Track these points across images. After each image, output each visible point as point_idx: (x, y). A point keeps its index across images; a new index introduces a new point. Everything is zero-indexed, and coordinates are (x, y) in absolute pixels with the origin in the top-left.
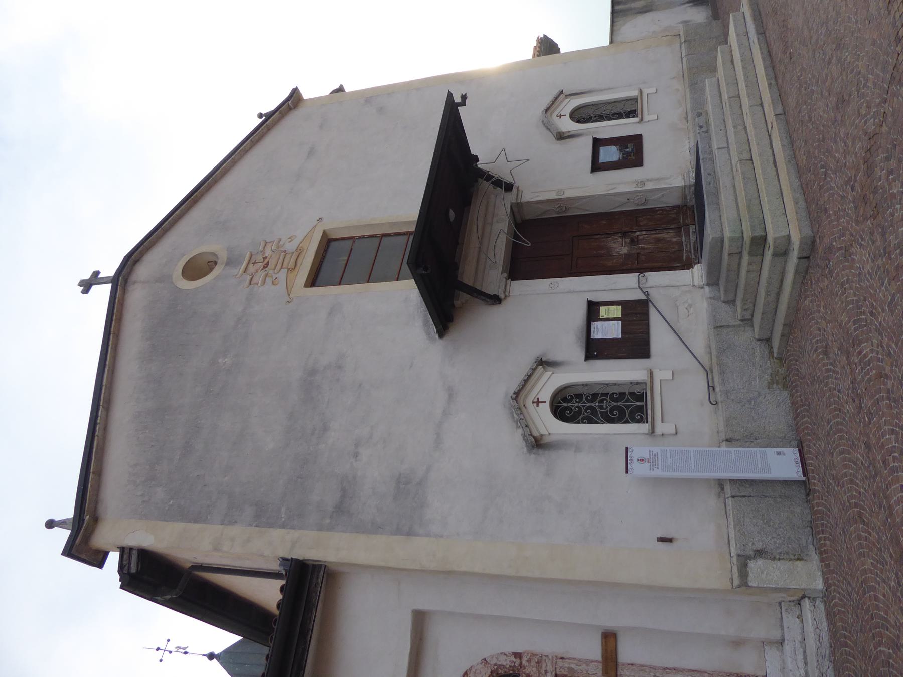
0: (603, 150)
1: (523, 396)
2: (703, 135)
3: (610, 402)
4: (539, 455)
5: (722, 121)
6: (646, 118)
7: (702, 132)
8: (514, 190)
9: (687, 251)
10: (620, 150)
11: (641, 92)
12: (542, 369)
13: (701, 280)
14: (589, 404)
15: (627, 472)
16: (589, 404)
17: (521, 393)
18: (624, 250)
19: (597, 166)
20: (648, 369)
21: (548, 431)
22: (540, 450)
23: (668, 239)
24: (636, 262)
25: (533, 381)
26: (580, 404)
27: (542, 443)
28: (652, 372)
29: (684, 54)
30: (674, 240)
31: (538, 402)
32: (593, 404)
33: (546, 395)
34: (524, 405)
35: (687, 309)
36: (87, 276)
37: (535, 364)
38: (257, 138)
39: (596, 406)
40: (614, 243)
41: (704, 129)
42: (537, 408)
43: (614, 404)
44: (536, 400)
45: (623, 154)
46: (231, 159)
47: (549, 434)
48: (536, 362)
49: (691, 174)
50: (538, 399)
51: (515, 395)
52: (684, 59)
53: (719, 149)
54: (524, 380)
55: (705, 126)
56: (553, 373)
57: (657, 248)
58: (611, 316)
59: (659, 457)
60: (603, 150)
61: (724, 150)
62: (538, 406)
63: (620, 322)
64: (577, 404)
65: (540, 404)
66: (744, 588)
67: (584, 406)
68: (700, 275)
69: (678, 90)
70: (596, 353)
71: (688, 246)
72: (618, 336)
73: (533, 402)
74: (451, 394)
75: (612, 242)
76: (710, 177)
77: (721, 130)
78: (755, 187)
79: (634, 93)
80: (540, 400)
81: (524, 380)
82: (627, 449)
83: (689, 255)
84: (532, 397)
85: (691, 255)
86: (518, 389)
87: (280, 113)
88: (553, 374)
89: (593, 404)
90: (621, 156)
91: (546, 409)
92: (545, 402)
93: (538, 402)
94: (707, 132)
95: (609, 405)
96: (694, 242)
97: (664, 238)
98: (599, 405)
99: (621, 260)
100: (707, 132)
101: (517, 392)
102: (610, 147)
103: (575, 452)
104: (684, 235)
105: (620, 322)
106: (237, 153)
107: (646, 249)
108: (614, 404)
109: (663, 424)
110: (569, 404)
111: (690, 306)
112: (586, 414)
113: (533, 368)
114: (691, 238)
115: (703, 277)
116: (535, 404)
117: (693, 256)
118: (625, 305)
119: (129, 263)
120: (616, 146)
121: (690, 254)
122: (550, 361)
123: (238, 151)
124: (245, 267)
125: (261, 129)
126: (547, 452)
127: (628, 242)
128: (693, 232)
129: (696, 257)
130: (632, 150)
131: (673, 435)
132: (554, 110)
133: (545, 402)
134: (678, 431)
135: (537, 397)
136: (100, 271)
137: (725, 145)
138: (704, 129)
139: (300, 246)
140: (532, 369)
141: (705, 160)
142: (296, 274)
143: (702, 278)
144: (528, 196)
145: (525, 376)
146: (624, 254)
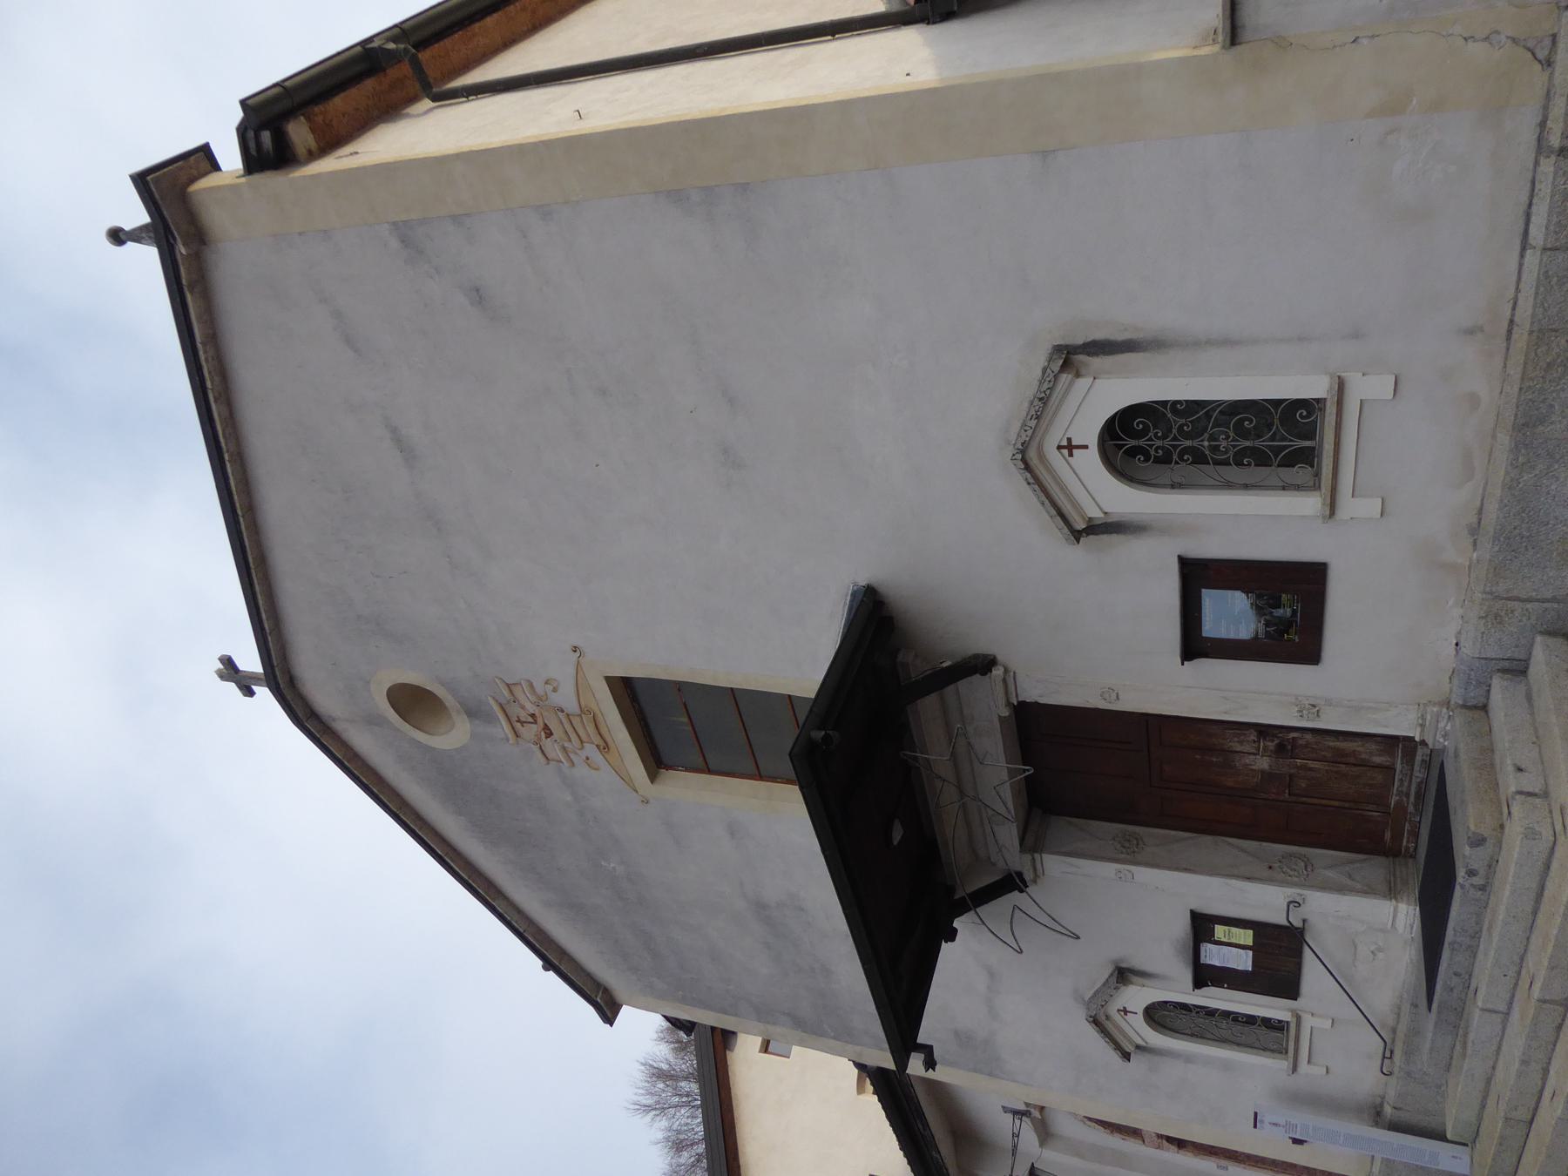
0: (1211, 600)
2: (1472, 891)
5: (1516, 959)
6: (1349, 506)
7: (1472, 885)
8: (997, 672)
9: (1400, 793)
10: (1259, 610)
11: (1341, 387)
13: (1408, 929)
15: (1255, 1126)
18: (1263, 763)
19: (1194, 645)
21: (1101, 509)
23: (1363, 756)
24: (1287, 791)
25: (1051, 413)
28: (1300, 1017)
29: (1537, 234)
30: (1377, 760)
31: (1070, 447)
33: (1088, 430)
34: (1107, 1016)
35: (1372, 952)
36: (232, 687)
38: (217, 379)
40: (1241, 743)
41: (1477, 881)
44: (1065, 443)
45: (1267, 624)
46: (227, 463)
47: (1106, 513)
49: (1441, 725)
50: (1069, 440)
52: (1532, 259)
53: (1483, 1010)
55: (1482, 872)
56: (1095, 378)
57: (1336, 772)
58: (1233, 941)
59: (1298, 1128)
60: (1211, 600)
61: (1494, 1015)
62: (1071, 455)
63: (1250, 953)
64: (1159, 443)
65: (1075, 451)
66: (1486, 44)
68: (1408, 922)
69: (1473, 400)
71: (1406, 784)
72: (1249, 936)
74: (992, 974)
75: (1236, 739)
76: (1455, 980)
77: (1505, 975)
78: (1515, 1159)
79: (1312, 387)
82: (1256, 1114)
83: (1402, 800)
84: (1055, 437)
85: (1408, 803)
87: (192, 288)
90: (1261, 626)
91: (1090, 462)
92: (1086, 447)
93: (1070, 447)
94: (1483, 888)
95: (1234, 446)
96: (1421, 782)
97: (1354, 751)
99: (1255, 780)
100: (1483, 888)
102: (1230, 592)
104: (1402, 759)
105: (1250, 953)
106: (223, 445)
107: (1311, 769)
111: (1380, 950)
114: (1416, 774)
115: (1415, 926)
116: (1065, 452)
117: (1411, 808)
118: (1257, 927)
119: (289, 697)
120: (1247, 593)
121: (1405, 799)
123: (222, 440)
124: (510, 728)
125: (204, 363)
127: (1272, 748)
128: (1423, 760)
129: (1416, 810)
130: (1294, 612)
132: (1043, 435)
133: (1086, 447)
136: (255, 697)
137: (1502, 1007)
138: (1477, 881)
139: (583, 707)
141: (1456, 946)
142: (617, 755)
143: (1412, 928)
144: (1035, 690)
146: (1263, 772)
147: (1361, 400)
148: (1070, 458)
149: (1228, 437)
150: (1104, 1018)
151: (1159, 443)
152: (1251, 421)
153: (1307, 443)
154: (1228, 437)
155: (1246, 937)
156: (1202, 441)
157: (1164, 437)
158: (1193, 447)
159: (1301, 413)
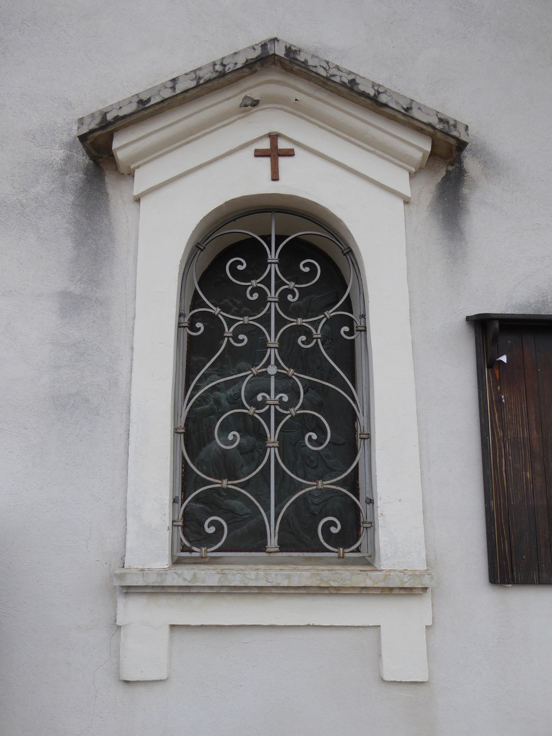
1: (293, 94)
3: (279, 417)
4: (63, 172)
12: (418, 156)
14: (272, 340)
16: (272, 340)
17: (302, 85)
20: (426, 581)
22: (81, 175)
26: (273, 308)
27: (107, 179)
32: (273, 353)
34: (255, 103)
37: (434, 121)
39: (268, 363)
42: (250, 152)
43: (273, 437)
44: (282, 145)
47: (138, 200)
48: (441, 120)
50: (289, 153)
51: (280, 51)
54: (353, 81)
56: (406, 202)
62: (259, 154)
63: (182, 435)
64: (273, 295)
65: (266, 162)
67: (265, 321)
70: (504, 359)
73: (274, 137)
80: (283, 161)
81: (353, 81)
86: (311, 62)
88: (400, 203)
89: (273, 353)
92: (275, 177)
95: (266, 416)
98: (265, 375)
101: (294, 61)
103: (65, 294)
108: (273, 437)
109: (167, 629)
110: (273, 269)
112: (228, 332)
113: (415, 113)
116: (266, 145)
122: (465, 191)
126: (70, 198)
131: (118, 672)
133: (275, 177)
134: (141, 690)
135: (297, 150)
140: (408, 109)
145: (374, 85)
147: (379, 626)
148: (252, 153)
149: (286, 406)
150: (255, 94)
151: (273, 295)
152: (318, 443)
153: (273, 542)
154: (286, 406)
155: (363, 324)
156: (277, 363)
157: (283, 301)
158: (264, 345)
159: (336, 526)
